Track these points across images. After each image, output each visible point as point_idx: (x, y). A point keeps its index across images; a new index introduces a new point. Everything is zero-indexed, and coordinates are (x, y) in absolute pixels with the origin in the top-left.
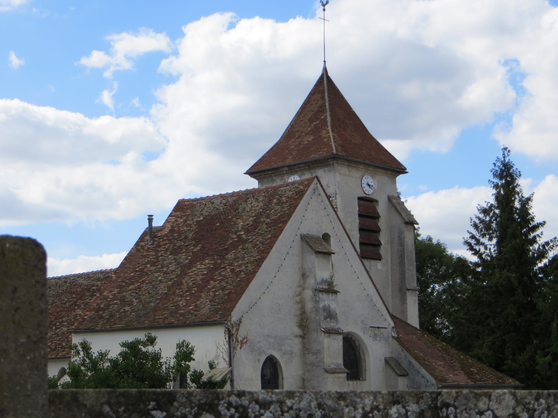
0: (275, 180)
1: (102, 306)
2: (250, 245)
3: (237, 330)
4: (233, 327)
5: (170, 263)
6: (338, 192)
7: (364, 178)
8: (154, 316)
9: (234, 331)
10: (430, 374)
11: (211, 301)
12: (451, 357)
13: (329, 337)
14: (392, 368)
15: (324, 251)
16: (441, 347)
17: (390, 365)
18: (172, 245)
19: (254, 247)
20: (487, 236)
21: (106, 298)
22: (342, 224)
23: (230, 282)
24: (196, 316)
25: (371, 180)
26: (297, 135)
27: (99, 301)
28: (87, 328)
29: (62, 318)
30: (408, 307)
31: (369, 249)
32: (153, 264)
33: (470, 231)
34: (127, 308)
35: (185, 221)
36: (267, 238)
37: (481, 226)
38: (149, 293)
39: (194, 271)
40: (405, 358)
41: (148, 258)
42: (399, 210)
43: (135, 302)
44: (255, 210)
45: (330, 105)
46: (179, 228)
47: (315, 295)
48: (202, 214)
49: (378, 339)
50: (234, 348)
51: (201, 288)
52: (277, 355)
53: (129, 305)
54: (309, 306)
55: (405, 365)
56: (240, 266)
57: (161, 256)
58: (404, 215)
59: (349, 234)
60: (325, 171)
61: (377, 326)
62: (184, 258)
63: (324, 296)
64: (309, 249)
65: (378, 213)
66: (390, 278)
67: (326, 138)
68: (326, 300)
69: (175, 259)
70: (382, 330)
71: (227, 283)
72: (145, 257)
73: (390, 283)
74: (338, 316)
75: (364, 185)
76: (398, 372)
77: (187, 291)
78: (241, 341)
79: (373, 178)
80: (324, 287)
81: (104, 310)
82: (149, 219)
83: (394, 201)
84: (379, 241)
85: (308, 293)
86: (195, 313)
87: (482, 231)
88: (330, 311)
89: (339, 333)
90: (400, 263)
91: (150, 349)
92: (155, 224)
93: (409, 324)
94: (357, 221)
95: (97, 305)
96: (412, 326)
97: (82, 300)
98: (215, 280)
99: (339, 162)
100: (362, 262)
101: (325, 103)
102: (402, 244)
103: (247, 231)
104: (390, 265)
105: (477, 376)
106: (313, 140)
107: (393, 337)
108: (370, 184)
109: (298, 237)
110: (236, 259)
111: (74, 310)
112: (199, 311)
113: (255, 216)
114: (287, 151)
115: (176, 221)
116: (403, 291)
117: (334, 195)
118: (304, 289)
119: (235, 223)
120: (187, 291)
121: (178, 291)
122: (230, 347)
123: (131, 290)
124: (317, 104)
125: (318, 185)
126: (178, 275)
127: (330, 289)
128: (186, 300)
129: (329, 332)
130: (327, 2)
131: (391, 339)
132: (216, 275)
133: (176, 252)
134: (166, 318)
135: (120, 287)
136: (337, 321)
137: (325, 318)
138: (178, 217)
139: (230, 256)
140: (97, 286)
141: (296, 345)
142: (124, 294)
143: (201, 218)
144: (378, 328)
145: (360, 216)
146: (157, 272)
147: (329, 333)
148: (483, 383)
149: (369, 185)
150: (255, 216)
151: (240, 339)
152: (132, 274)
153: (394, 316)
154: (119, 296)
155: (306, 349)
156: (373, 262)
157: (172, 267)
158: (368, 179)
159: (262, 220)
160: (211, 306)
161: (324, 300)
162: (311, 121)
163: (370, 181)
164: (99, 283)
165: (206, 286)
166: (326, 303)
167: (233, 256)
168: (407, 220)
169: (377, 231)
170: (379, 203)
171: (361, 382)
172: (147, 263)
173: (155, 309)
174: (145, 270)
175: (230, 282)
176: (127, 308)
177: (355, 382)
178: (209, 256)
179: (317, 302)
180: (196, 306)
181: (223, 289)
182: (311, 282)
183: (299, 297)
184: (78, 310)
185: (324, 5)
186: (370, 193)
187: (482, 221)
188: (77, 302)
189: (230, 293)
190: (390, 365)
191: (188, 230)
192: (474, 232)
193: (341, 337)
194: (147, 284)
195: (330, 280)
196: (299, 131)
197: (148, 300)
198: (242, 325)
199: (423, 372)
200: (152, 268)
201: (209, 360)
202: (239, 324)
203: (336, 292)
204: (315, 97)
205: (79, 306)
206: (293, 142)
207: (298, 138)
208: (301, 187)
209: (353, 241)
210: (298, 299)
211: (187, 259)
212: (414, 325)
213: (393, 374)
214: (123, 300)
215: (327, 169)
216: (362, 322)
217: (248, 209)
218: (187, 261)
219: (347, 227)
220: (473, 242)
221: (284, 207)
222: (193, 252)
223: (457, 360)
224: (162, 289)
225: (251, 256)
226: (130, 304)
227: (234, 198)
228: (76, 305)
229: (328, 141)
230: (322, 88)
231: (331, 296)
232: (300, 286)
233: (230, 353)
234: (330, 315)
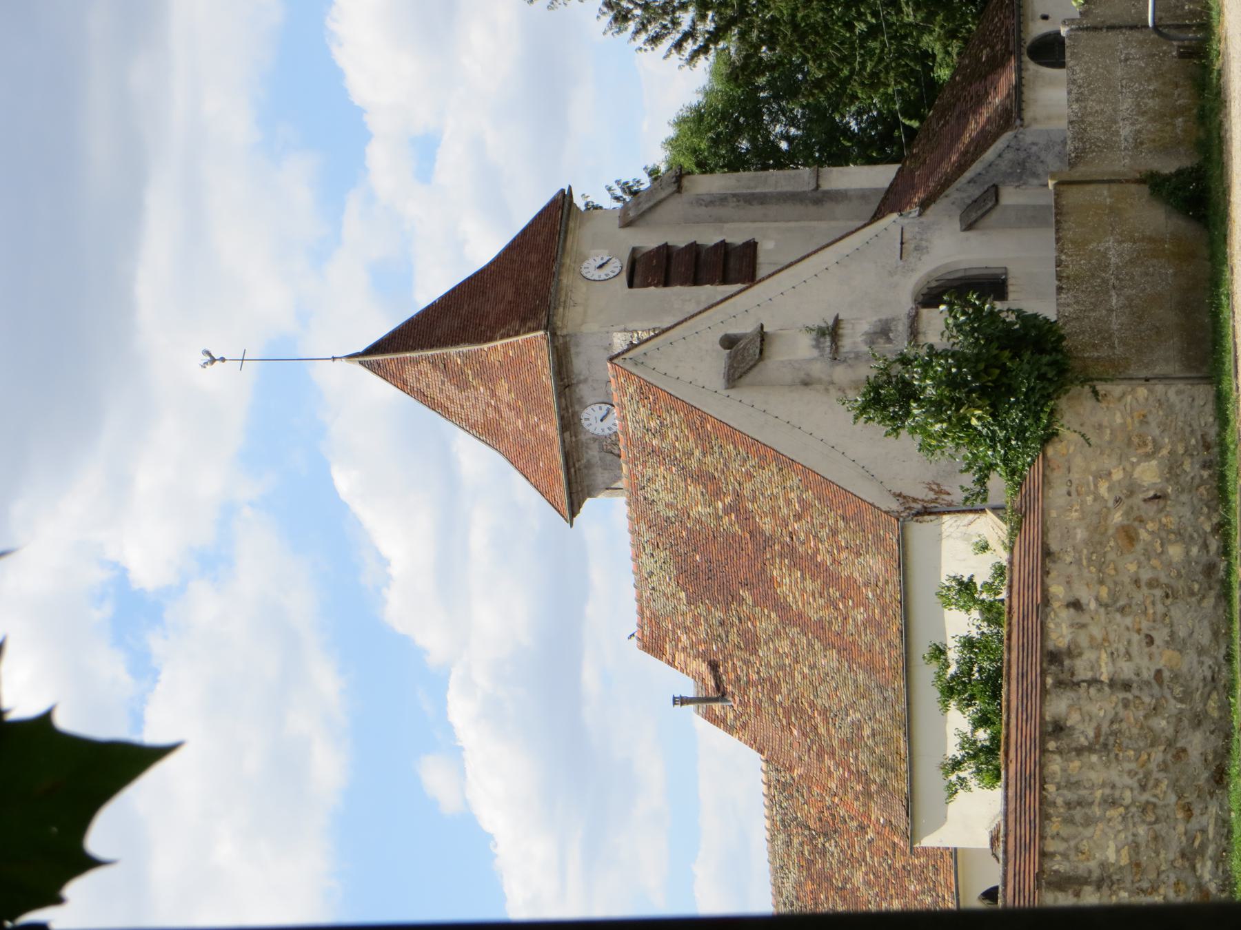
0: (588, 461)
1: (859, 788)
2: (748, 486)
3: (915, 500)
4: (910, 508)
5: (776, 651)
6: (622, 327)
7: (589, 276)
8: (884, 669)
9: (918, 506)
10: (995, 141)
11: (859, 554)
12: (959, 100)
13: (924, 333)
14: (983, 215)
15: (758, 344)
16: (939, 120)
17: (976, 221)
18: (738, 653)
19: (752, 477)
20: (677, 14)
21: (843, 782)
22: (686, 320)
23: (822, 519)
24: (887, 582)
25: (591, 261)
26: (491, 414)
27: (850, 796)
28: (904, 813)
30: (854, 186)
31: (733, 265)
32: (775, 688)
33: (664, 54)
34: (867, 732)
35: (687, 630)
36: (733, 453)
37: (653, 29)
38: (836, 689)
39: (794, 597)
40: (962, 191)
41: (761, 701)
42: (651, 203)
43: (854, 716)
44: (672, 482)
45: (431, 347)
46: (699, 642)
47: (845, 361)
49: (924, 244)
50: (950, 505)
51: (831, 579)
53: (860, 728)
55: (976, 192)
56: (789, 502)
57: (758, 673)
58: (663, 195)
59: (706, 306)
60: (578, 354)
61: (899, 246)
62: (765, 624)
63: (847, 344)
64: (756, 370)
65: (659, 248)
66: (792, 224)
67: (506, 354)
68: (853, 339)
69: (766, 643)
70: (906, 236)
71: (822, 526)
72: (758, 708)
73: (802, 224)
74: (884, 317)
75: (602, 274)
76: (990, 204)
77: (836, 608)
78: (936, 493)
79: (585, 258)
80: (828, 344)
81: (868, 782)
82: (682, 704)
83: (632, 214)
84: (716, 245)
86: (880, 584)
87: (664, 27)
88: (875, 333)
89: (917, 314)
90: (762, 203)
91: (953, 655)
92: (691, 693)
93: (891, 185)
94: (677, 289)
95: (857, 799)
96: (895, 178)
97: (832, 876)
99: (559, 324)
100: (760, 281)
101: (427, 358)
102: (722, 200)
103: (718, 494)
104: (764, 225)
105: (998, 47)
106: (508, 381)
107: (920, 215)
108: (597, 262)
109: (732, 392)
110: (773, 513)
112: (877, 577)
113: (686, 480)
114: (529, 435)
115: (685, 649)
116: (819, 198)
117: (629, 335)
118: (832, 383)
119: (699, 521)
120: (836, 608)
121: (835, 627)
122: (949, 512)
123: (828, 730)
124: (426, 374)
125: (627, 356)
126: (802, 631)
127: (832, 333)
128: (856, 605)
130: (209, 353)
131: (923, 219)
132: (806, 551)
133: (751, 643)
134: (889, 644)
135: (820, 756)
136: (893, 319)
137: (889, 340)
138: (677, 646)
139: (767, 525)
140: (801, 844)
142: (835, 743)
143: (683, 595)
144: (902, 243)
145: (666, 284)
146: (793, 677)
148: (1011, 38)
149: (601, 267)
150: (686, 480)
151: (932, 495)
152: (795, 732)
153: (875, 215)
154: (840, 753)
156: (762, 258)
157: (784, 646)
158: (590, 269)
159: (695, 465)
160: (867, 552)
161: (854, 343)
162: (463, 385)
164: (796, 841)
165: (827, 569)
166: (859, 339)
167: (767, 520)
168: (674, 188)
169: (694, 248)
170: (637, 245)
171: (1010, 276)
172: (772, 700)
173: (871, 669)
174: (787, 704)
175: (822, 519)
176: (867, 732)
177: (1011, 288)
178: (764, 570)
179: (858, 356)
180: (867, 584)
181: (834, 532)
182: (819, 369)
184: (855, 880)
185: (213, 360)
186: (618, 264)
187: (643, 27)
188: (837, 888)
190: (976, 221)
191: (706, 620)
192: (667, 43)
193: (925, 312)
194: (816, 696)
195: (814, 333)
196: (484, 413)
197: (851, 688)
198: (904, 493)
199: (990, 154)
201: (972, 554)
202: (904, 497)
203: (837, 321)
204: (411, 381)
205: (846, 880)
206: (508, 423)
207: (499, 412)
208: (631, 390)
209: (719, 298)
211: (769, 616)
212: (893, 175)
213: (994, 215)
214: (848, 744)
215: (573, 350)
216: (891, 274)
217: (669, 498)
218: (773, 615)
219: (693, 308)
220: (690, 46)
221: (672, 423)
222: (756, 604)
223: (964, 88)
224: (828, 661)
225: (770, 482)
226: (857, 725)
227: (644, 527)
228: (843, 888)
229: (513, 348)
230: (393, 366)
231: (846, 330)
232: (827, 390)
233: (959, 512)
234: (883, 331)
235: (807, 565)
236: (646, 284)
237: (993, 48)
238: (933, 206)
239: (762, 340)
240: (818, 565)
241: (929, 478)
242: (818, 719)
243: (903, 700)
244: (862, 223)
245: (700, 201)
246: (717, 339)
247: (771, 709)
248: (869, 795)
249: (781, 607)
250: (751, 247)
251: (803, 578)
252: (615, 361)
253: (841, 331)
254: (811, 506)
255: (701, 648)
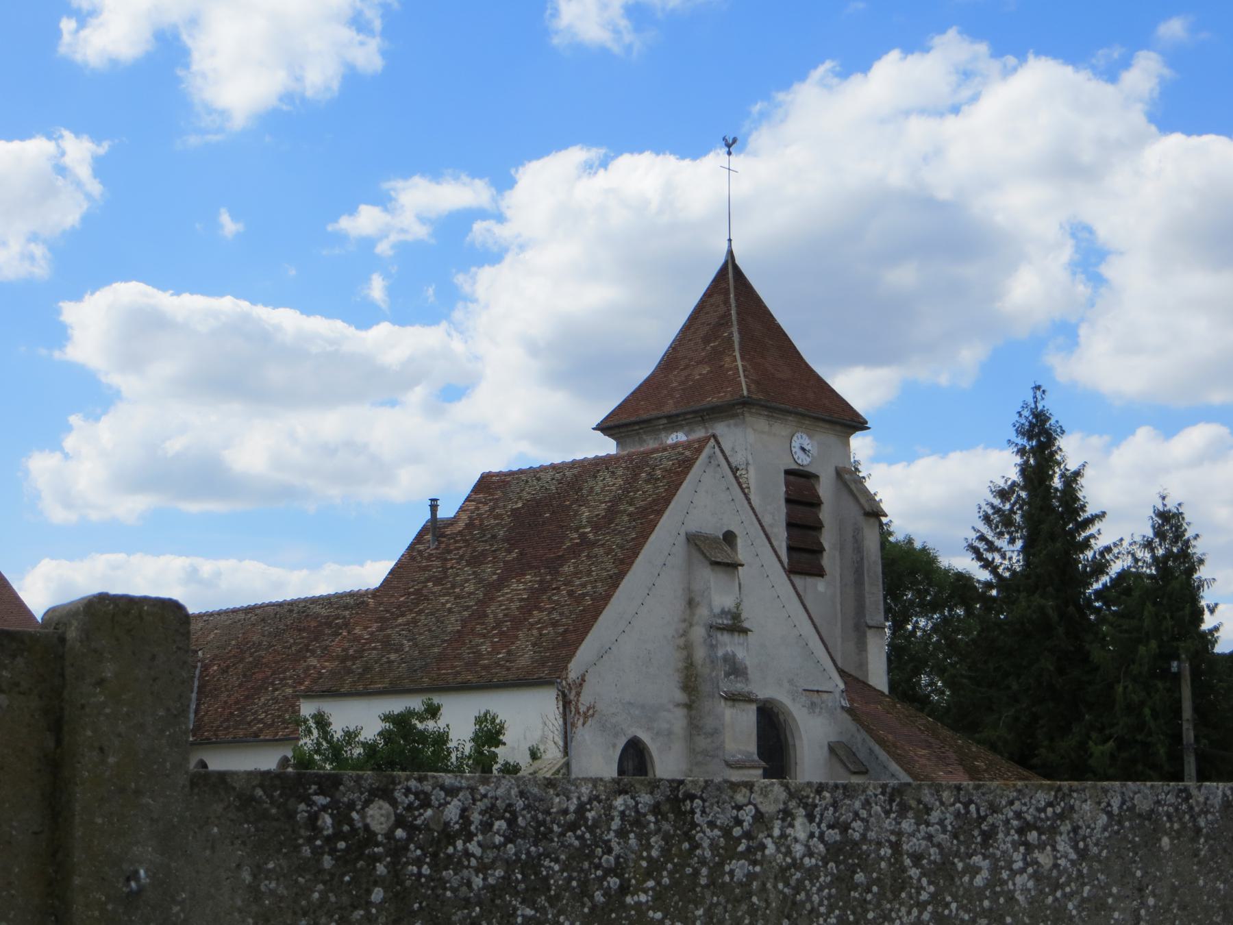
3: (578, 694)
4: (570, 689)
5: (467, 581)
7: (795, 438)
9: (572, 696)
11: (534, 645)
14: (841, 761)
18: (469, 550)
20: (1007, 536)
21: (357, 639)
29: (284, 672)
30: (870, 657)
31: (803, 557)
32: (438, 581)
34: (393, 656)
35: (492, 509)
36: (629, 538)
38: (430, 630)
40: (863, 743)
44: (611, 491)
47: (710, 636)
48: (520, 498)
49: (817, 710)
50: (573, 725)
51: (517, 623)
52: (645, 737)
53: (396, 651)
54: (700, 654)
55: (862, 755)
56: (584, 585)
58: (863, 501)
59: (769, 532)
60: (729, 426)
62: (489, 571)
63: (725, 638)
66: (839, 607)
67: (731, 369)
68: (729, 644)
70: (825, 696)
71: (561, 614)
72: (426, 569)
75: (796, 449)
79: (810, 437)
81: (354, 658)
83: (847, 476)
84: (821, 544)
85: (698, 633)
91: (430, 725)
92: (441, 514)
94: (783, 508)
95: (343, 650)
96: (875, 689)
98: (541, 610)
101: (729, 310)
103: (596, 528)
104: (838, 584)
107: (843, 707)
109: (682, 538)
110: (577, 574)
111: (305, 659)
115: (478, 508)
116: (860, 629)
118: (691, 625)
120: (494, 628)
121: (478, 628)
125: (717, 449)
127: (735, 625)
129: (734, 698)
131: (839, 710)
134: (459, 673)
136: (747, 680)
137: (727, 675)
140: (344, 617)
141: (677, 720)
142: (389, 631)
143: (520, 505)
145: (788, 501)
146: (444, 595)
147: (734, 700)
149: (803, 449)
151: (582, 709)
155: (694, 727)
156: (810, 580)
157: (470, 587)
158: (801, 440)
159: (622, 508)
162: (706, 340)
163: (807, 442)
168: (868, 508)
169: (818, 527)
173: (441, 658)
174: (425, 592)
176: (393, 656)
178: (531, 568)
179: (713, 647)
180: (509, 653)
181: (555, 624)
182: (703, 612)
183: (683, 639)
186: (805, 463)
187: (997, 511)
189: (566, 631)
192: (985, 529)
193: (754, 707)
194: (427, 615)
196: (685, 357)
197: (428, 643)
198: (585, 685)
200: (435, 589)
201: (529, 744)
202: (581, 685)
203: (745, 631)
204: (712, 300)
205: (313, 652)
208: (687, 453)
209: (775, 543)
210: (681, 641)
212: (878, 688)
214: (387, 644)
215: (732, 422)
216: (791, 682)
217: (598, 489)
218: (495, 577)
219: (767, 520)
220: (982, 546)
226: (399, 649)
228: (308, 650)
231: (737, 638)
232: (685, 621)
234: (735, 669)
235: (532, 603)
236: (787, 484)
237: (985, 771)
238: (849, 718)
239: (728, 565)
240: (530, 612)
241: (599, 707)
242: (409, 617)
243: (412, 686)
244: (840, 665)
245: (857, 531)
246: (732, 528)
247: (422, 579)
248: (343, 661)
249: (501, 583)
250: (820, 573)
251: (522, 600)
252: (712, 440)
253: (736, 634)
254: (579, 604)
255: (477, 522)
